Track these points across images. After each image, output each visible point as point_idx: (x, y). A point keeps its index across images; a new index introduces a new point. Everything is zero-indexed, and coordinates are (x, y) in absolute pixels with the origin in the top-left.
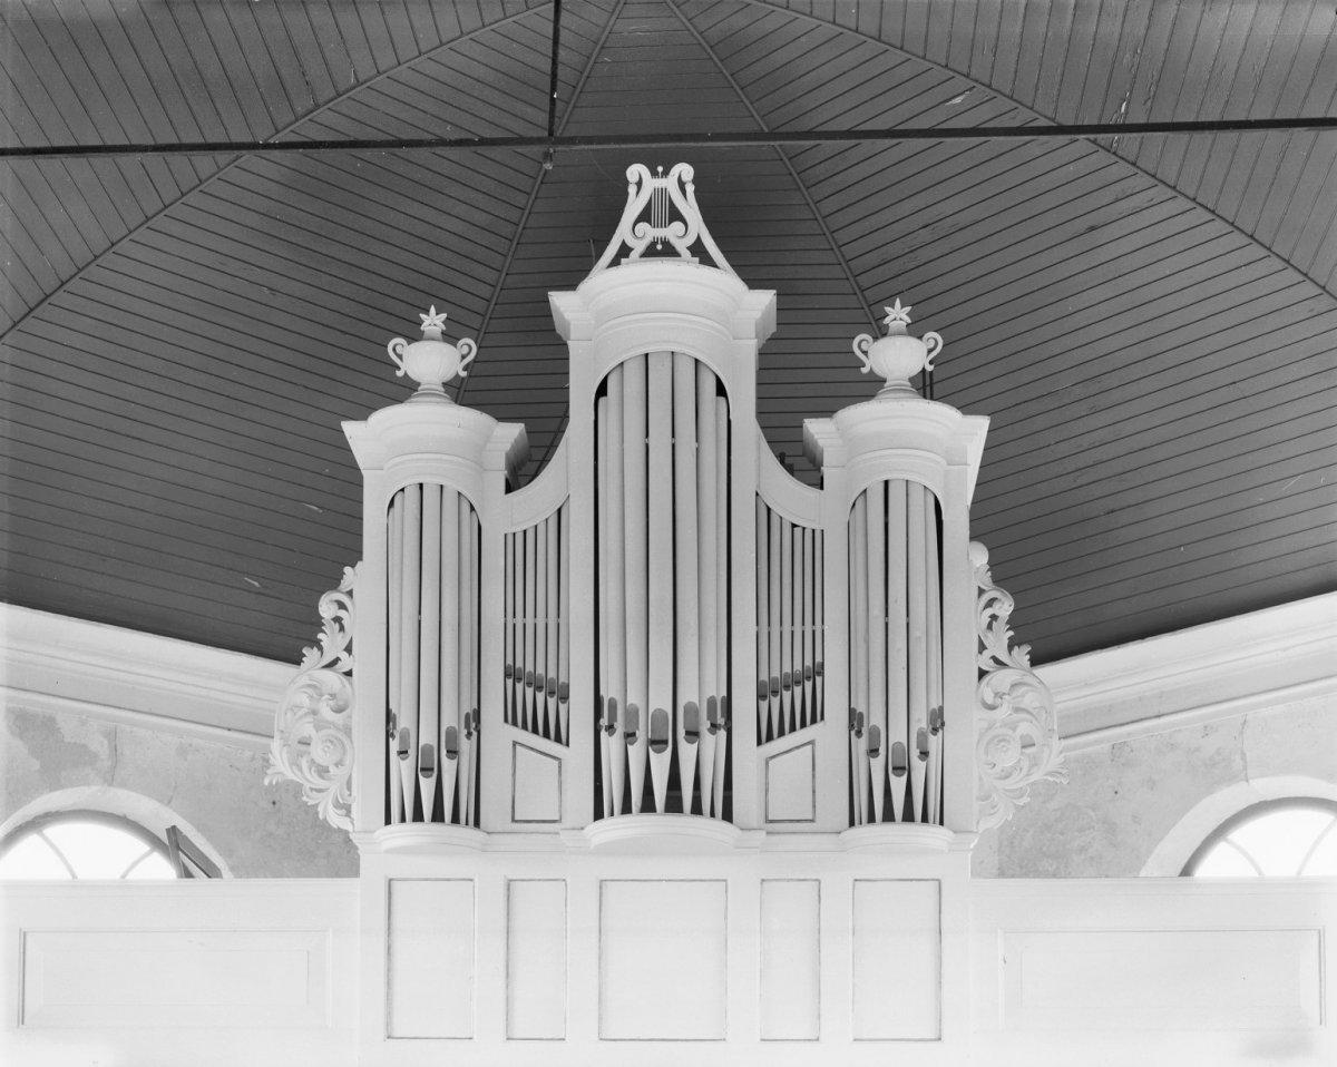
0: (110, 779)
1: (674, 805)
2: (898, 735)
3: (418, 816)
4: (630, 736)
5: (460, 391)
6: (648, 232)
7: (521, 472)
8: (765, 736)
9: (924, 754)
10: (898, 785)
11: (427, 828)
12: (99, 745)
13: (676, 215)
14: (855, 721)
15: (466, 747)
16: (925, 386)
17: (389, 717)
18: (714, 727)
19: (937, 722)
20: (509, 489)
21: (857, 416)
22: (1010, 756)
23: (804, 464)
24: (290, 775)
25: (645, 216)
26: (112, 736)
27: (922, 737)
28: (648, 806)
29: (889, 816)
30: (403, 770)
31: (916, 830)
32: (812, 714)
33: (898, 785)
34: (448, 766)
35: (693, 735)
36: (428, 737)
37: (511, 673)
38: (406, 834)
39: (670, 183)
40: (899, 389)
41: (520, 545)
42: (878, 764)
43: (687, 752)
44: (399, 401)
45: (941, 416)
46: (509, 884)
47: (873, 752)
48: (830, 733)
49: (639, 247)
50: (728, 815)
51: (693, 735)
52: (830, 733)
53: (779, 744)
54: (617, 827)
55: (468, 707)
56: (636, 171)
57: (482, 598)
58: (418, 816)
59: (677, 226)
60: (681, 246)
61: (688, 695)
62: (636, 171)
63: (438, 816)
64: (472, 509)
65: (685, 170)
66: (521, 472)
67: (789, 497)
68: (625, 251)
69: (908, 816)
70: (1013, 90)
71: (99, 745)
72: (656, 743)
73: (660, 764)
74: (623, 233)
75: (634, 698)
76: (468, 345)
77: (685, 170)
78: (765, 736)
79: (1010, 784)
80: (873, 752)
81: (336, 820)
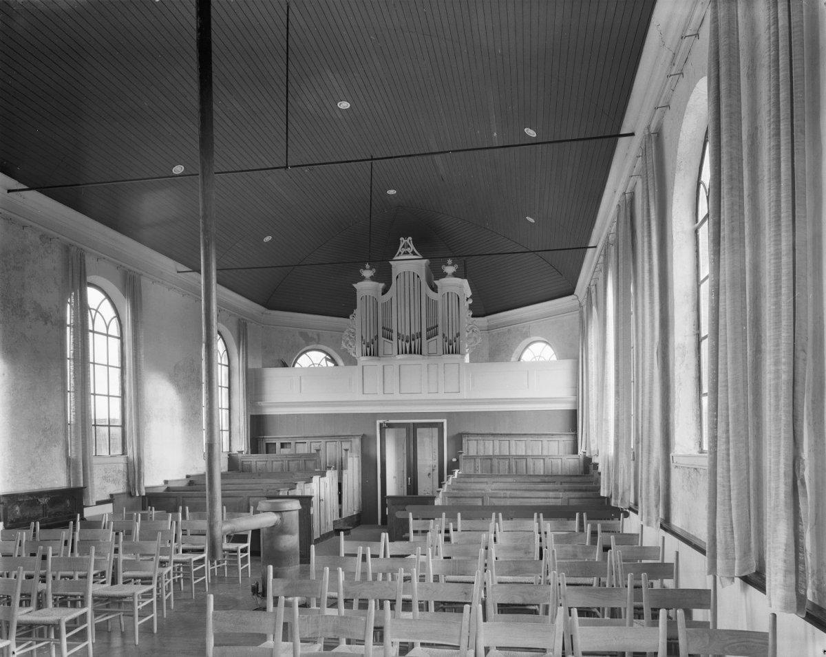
0: (318, 343)
1: (410, 352)
2: (450, 338)
3: (367, 355)
4: (403, 340)
5: (372, 279)
6: (404, 250)
7: (385, 291)
8: (428, 338)
9: (455, 341)
10: (451, 347)
11: (368, 357)
12: (316, 337)
13: (409, 246)
14: (444, 335)
15: (375, 342)
16: (455, 275)
17: (362, 337)
18: (418, 338)
19: (458, 335)
20: (383, 294)
21: (443, 281)
22: (472, 340)
23: (434, 289)
24: (346, 347)
25: (403, 247)
26: (318, 335)
27: (455, 339)
28: (406, 353)
29: (449, 353)
30: (364, 346)
31: (454, 356)
32: (436, 334)
33: (451, 347)
34: (372, 346)
35: (414, 340)
36: (368, 341)
37: (383, 328)
38: (364, 358)
39: (408, 241)
40: (450, 276)
41: (385, 305)
42: (447, 343)
43: (413, 343)
44: (361, 281)
45: (458, 280)
46: (384, 366)
47: (446, 341)
48: (439, 337)
49: (402, 253)
50: (421, 354)
51: (414, 340)
52: (439, 337)
53: (430, 340)
54: (401, 356)
55: (375, 335)
56: (402, 239)
57: (701, 152)
58: (367, 355)
59: (409, 249)
60: (410, 252)
61: (413, 332)
62: (402, 239)
63: (370, 355)
64: (418, 277)
65: (410, 238)
66: (385, 291)
67: (432, 294)
68: (400, 253)
69: (452, 353)
70: (108, 363)
71: (316, 337)
72: (407, 341)
73: (408, 345)
74: (400, 250)
75: (403, 333)
76: (374, 270)
77: (410, 238)
78: (428, 338)
79: (472, 345)
80: (446, 341)
81: (353, 355)
